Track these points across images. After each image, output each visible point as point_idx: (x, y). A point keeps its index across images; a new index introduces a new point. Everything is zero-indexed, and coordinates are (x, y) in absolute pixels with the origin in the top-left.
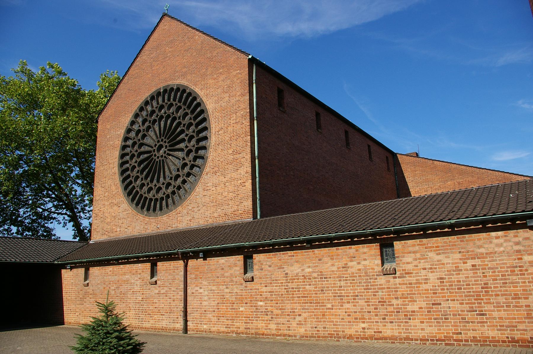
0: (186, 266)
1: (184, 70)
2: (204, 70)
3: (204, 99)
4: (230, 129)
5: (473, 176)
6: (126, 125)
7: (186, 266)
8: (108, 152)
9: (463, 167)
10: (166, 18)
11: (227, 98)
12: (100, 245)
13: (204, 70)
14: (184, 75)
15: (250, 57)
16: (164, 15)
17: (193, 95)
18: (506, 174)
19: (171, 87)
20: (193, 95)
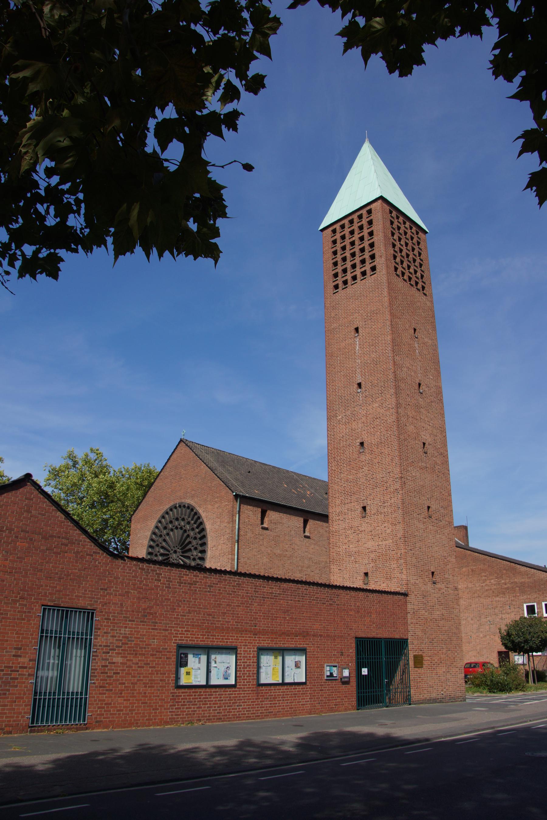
0: (294, 679)
1: (193, 492)
2: (206, 496)
3: (205, 520)
4: (220, 547)
5: (484, 564)
6: (152, 529)
7: (294, 679)
8: (138, 549)
9: (476, 554)
10: (182, 443)
11: (218, 523)
12: (258, 507)
13: (206, 496)
14: (193, 497)
15: (234, 494)
16: (181, 441)
17: (198, 515)
18: (512, 564)
19: (184, 504)
20: (198, 515)
